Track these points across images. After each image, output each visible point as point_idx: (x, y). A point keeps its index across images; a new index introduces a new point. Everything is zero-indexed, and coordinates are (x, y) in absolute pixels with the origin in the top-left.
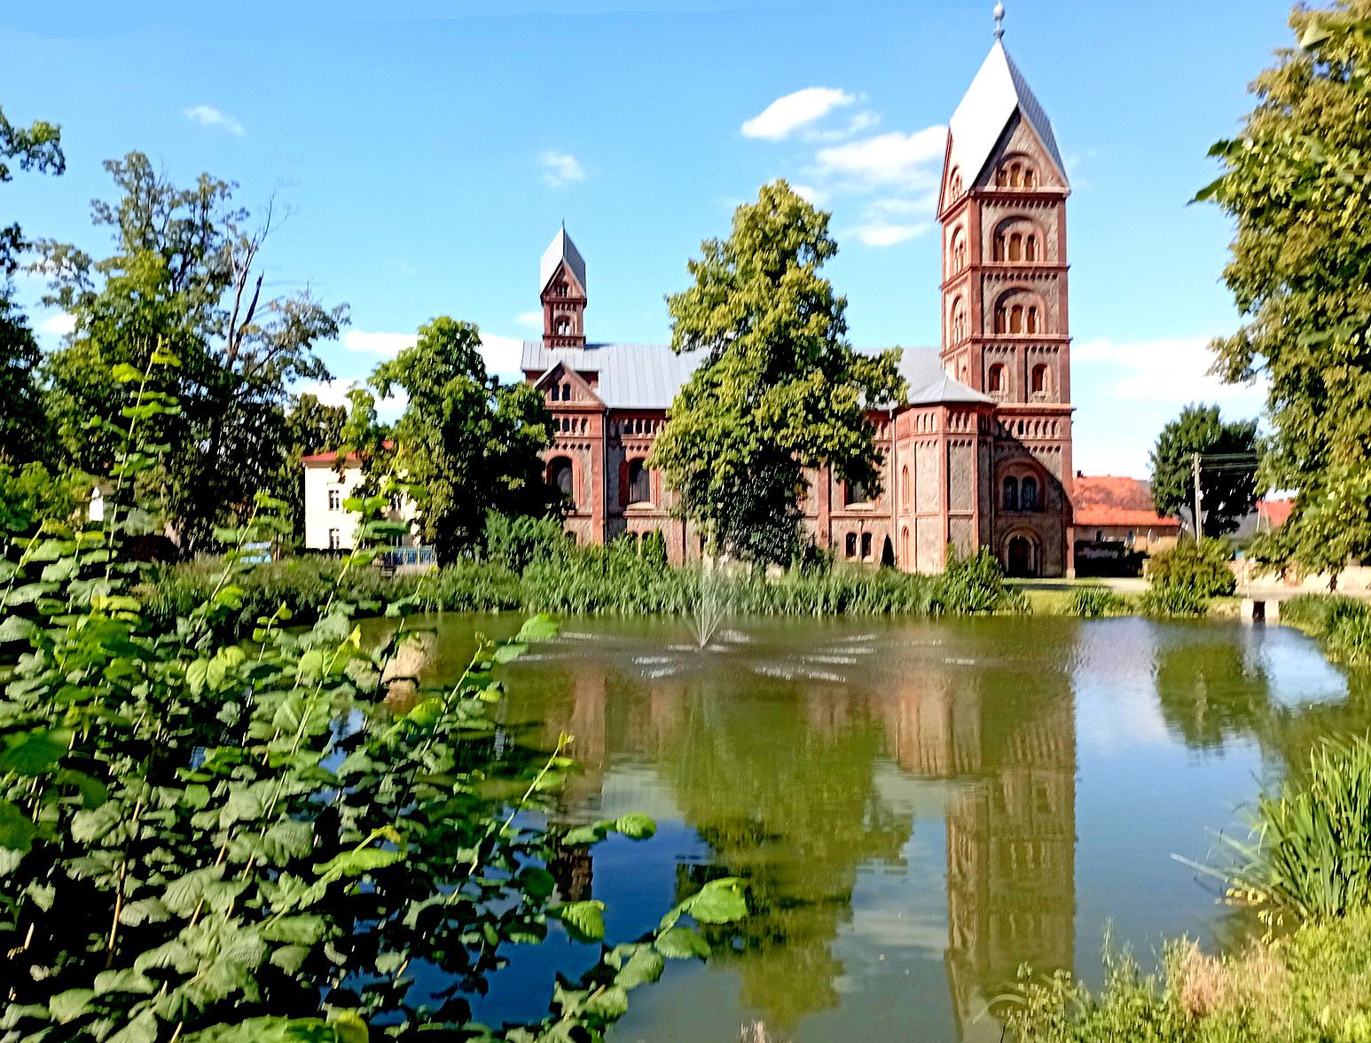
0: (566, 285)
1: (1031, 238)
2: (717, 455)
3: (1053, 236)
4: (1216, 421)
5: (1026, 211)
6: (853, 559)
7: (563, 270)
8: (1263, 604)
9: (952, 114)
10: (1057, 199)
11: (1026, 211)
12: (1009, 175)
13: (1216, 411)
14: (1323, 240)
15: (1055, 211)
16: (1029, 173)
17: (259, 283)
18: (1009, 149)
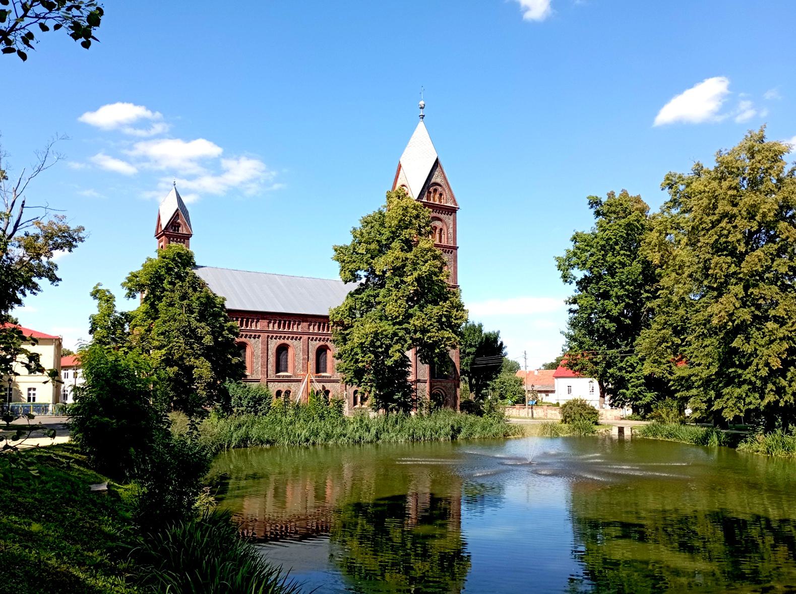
0: (179, 225)
1: (441, 230)
2: (391, 346)
3: (451, 230)
4: (481, 331)
5: (439, 215)
6: (357, 406)
7: (178, 215)
8: (623, 428)
9: (123, 102)
10: (452, 211)
11: (439, 215)
12: (432, 195)
13: (480, 326)
14: (688, 264)
15: (452, 217)
16: (441, 195)
17: (23, 206)
18: (433, 180)
